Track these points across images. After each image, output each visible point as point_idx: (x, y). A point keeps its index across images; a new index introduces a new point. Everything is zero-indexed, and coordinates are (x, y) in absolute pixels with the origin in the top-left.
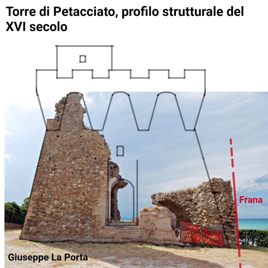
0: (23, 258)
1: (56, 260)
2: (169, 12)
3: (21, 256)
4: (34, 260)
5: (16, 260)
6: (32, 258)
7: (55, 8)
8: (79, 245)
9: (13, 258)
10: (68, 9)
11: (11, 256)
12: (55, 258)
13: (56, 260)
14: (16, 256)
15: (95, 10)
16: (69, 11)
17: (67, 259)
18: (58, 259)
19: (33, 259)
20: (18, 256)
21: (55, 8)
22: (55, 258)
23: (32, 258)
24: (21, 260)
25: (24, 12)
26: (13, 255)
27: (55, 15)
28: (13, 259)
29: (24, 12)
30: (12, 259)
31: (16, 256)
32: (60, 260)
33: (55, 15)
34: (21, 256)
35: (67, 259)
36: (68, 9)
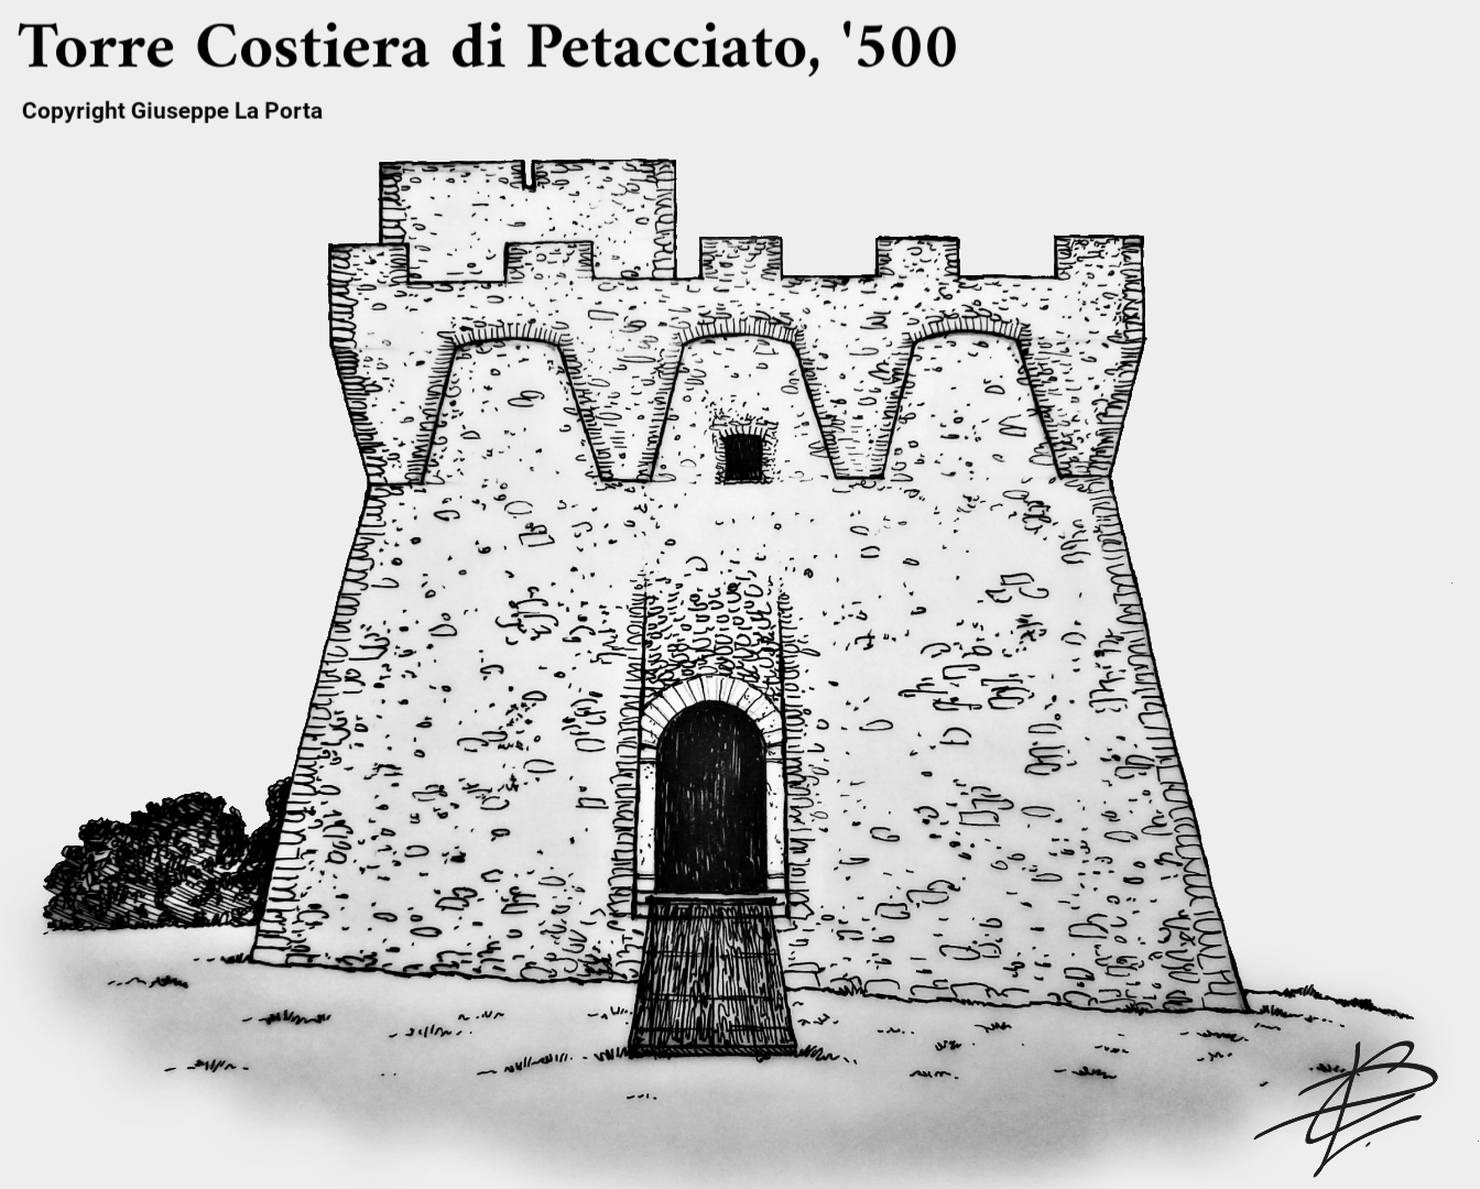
0: (167, 113)
1: (244, 117)
2: (300, 50)
3: (163, 108)
4: (194, 117)
5: (150, 117)
6: (188, 111)
7: (268, 104)
8: (1032, 406)
9: (143, 112)
10: (589, 37)
11: (138, 108)
12: (244, 112)
13: (244, 117)
14: (150, 108)
15: (711, 45)
16: (592, 47)
17: (271, 114)
18: (249, 114)
19: (190, 114)
20: (156, 108)
21: (268, 104)
22: (244, 112)
23: (188, 111)
24: (163, 116)
25: (113, 55)
26: (143, 105)
27: (268, 117)
28: (143, 115)
29: (113, 55)
30: (140, 114)
31: (150, 108)
32: (256, 116)
33: (268, 117)
34: (163, 108)
35: (271, 114)
36: (589, 37)
